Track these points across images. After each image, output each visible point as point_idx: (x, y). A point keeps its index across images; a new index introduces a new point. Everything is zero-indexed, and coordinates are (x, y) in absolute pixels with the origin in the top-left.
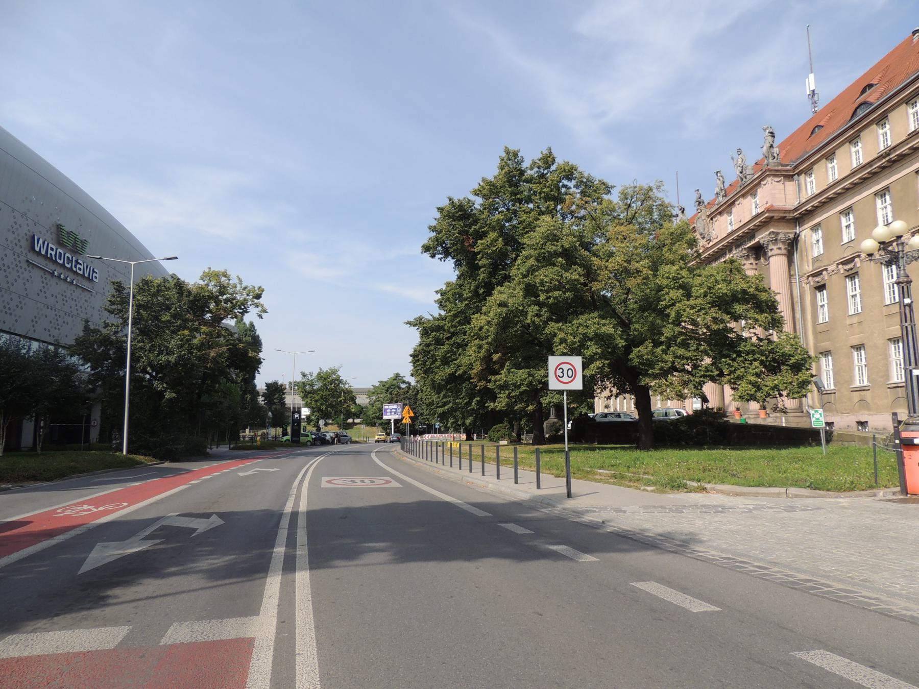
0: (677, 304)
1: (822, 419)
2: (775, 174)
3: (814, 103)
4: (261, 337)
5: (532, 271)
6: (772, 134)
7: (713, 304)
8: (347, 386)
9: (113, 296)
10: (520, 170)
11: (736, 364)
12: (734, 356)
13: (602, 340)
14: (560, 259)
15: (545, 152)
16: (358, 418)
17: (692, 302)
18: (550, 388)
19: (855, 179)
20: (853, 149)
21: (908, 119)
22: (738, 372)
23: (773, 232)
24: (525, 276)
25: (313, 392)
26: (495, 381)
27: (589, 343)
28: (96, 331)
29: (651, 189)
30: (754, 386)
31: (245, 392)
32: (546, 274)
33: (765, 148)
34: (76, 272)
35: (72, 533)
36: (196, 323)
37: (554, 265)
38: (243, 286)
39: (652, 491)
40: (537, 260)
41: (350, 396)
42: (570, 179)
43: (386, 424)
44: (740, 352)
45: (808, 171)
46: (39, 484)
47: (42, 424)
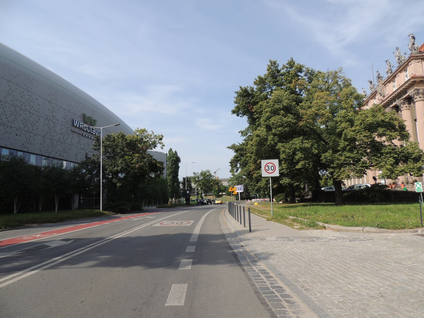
0: (345, 130)
5: (268, 118)
6: (414, 38)
7: (365, 129)
8: (214, 178)
10: (277, 70)
11: (380, 160)
12: (379, 155)
13: (304, 150)
15: (290, 60)
16: (224, 192)
17: (353, 128)
18: (263, 176)
22: (381, 164)
23: (416, 89)
24: (265, 121)
25: (199, 181)
26: (257, 173)
27: (297, 153)
28: (90, 158)
29: (336, 73)
30: (390, 171)
31: (174, 182)
33: (410, 45)
34: (92, 134)
35: (10, 246)
36: (131, 153)
38: (155, 135)
39: (297, 228)
40: (270, 113)
41: (217, 182)
42: (301, 72)
44: (383, 153)
46: (51, 224)
47: (82, 198)
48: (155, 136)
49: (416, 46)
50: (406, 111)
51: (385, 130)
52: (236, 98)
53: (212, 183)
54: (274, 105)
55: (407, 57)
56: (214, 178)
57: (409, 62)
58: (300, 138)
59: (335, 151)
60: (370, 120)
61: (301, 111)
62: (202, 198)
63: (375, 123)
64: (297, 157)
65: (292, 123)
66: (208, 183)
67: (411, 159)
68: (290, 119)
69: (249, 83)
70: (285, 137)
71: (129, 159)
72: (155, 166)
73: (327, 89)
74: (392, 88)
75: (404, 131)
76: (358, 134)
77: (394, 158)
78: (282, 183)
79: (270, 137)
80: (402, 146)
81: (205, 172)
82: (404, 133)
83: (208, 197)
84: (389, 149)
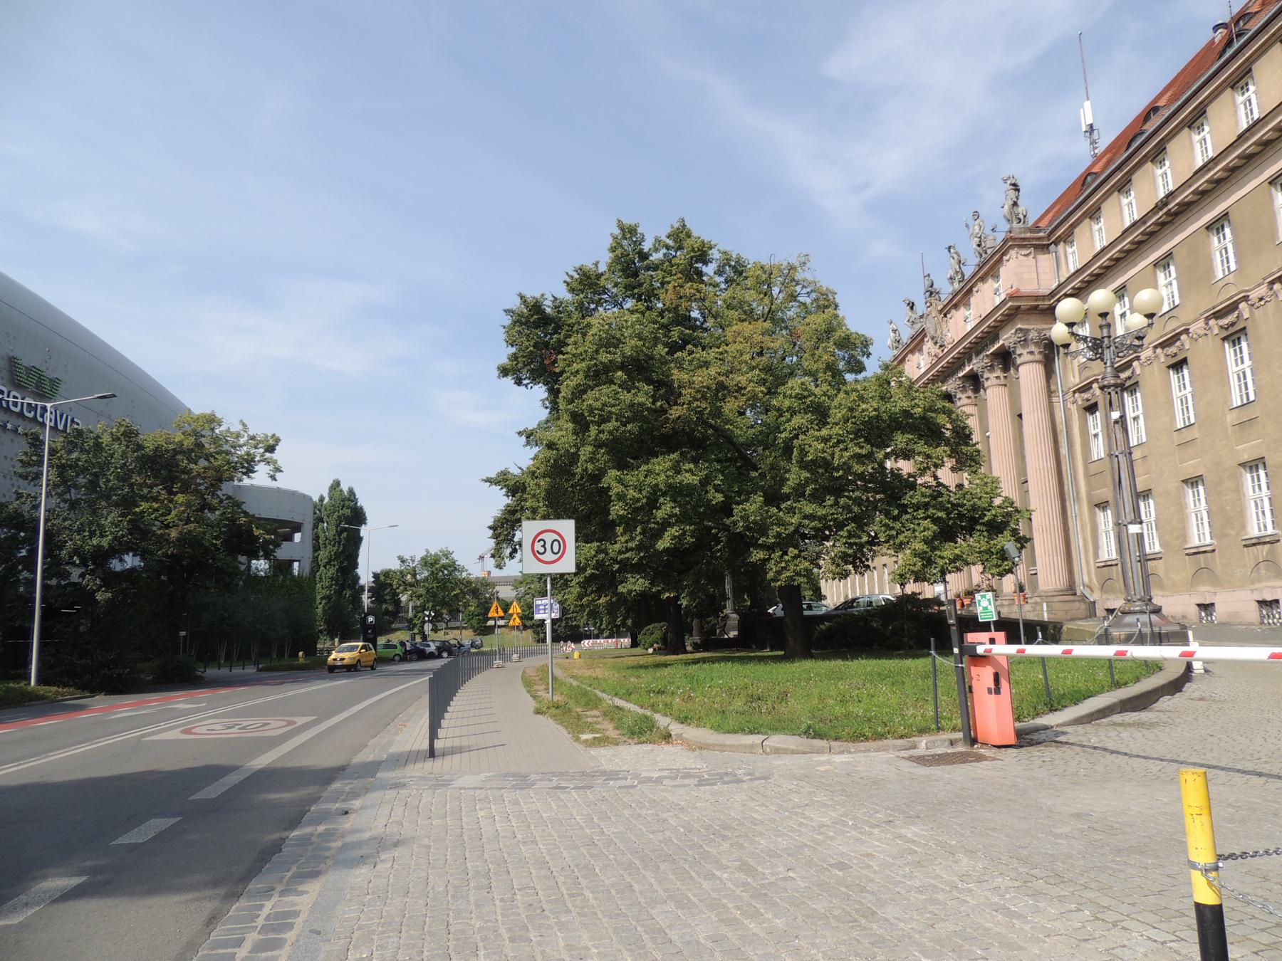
0: (801, 437)
1: (992, 608)
2: (1022, 243)
3: (1093, 142)
4: (366, 509)
6: (1016, 187)
8: (464, 575)
9: (26, 454)
11: (898, 525)
13: (680, 493)
14: (620, 373)
15: (676, 225)
17: (824, 432)
19: (1124, 244)
20: (1125, 201)
21: (1192, 149)
22: (901, 538)
23: (1020, 329)
24: (571, 402)
29: (792, 268)
31: (343, 587)
32: (597, 397)
37: (612, 382)
38: (251, 433)
43: (538, 626)
44: (905, 506)
45: (1067, 238)
48: (253, 438)
49: (1021, 209)
50: (996, 389)
51: (910, 440)
52: (508, 330)
53: (457, 591)
54: (597, 351)
55: (1000, 237)
56: (464, 575)
57: (1004, 254)
58: (672, 456)
59: (773, 498)
60: (869, 408)
61: (676, 374)
62: (424, 638)
63: (885, 417)
64: (660, 514)
65: (647, 409)
66: (444, 588)
67: (983, 524)
68: (641, 399)
69: (552, 288)
70: (626, 453)
71: (157, 510)
72: (248, 533)
73: (770, 315)
74: (962, 325)
75: (967, 444)
76: (837, 450)
77: (935, 521)
78: (625, 590)
79: (586, 451)
80: (960, 486)
81: (436, 555)
82: (965, 449)
83: (440, 636)
84: (923, 495)
